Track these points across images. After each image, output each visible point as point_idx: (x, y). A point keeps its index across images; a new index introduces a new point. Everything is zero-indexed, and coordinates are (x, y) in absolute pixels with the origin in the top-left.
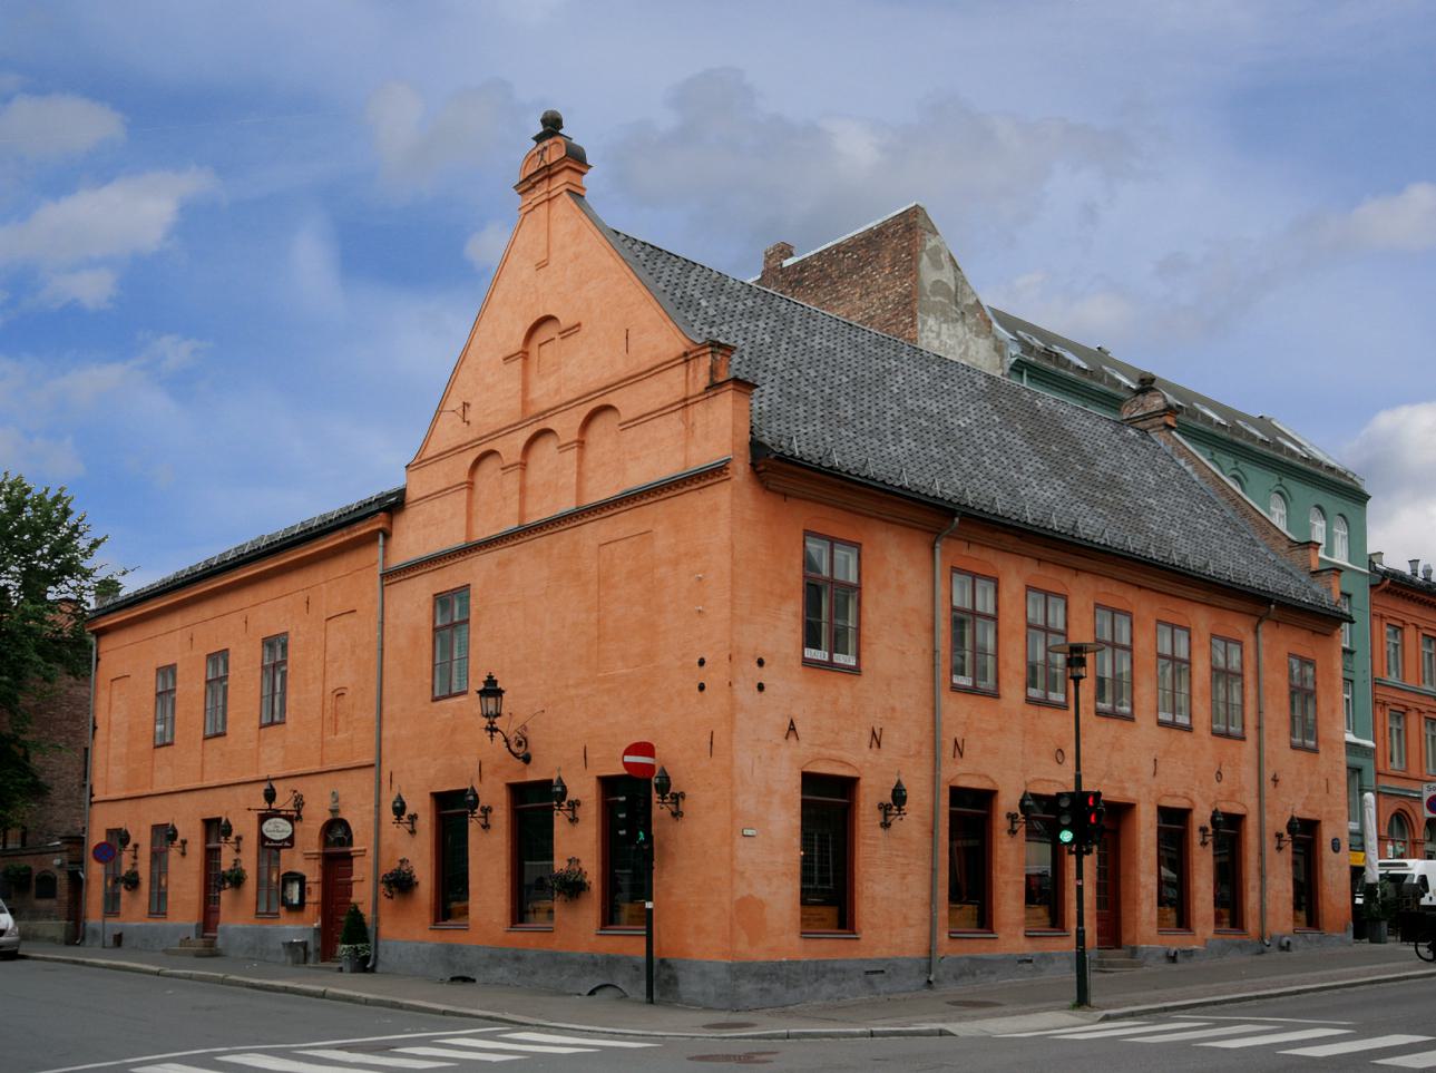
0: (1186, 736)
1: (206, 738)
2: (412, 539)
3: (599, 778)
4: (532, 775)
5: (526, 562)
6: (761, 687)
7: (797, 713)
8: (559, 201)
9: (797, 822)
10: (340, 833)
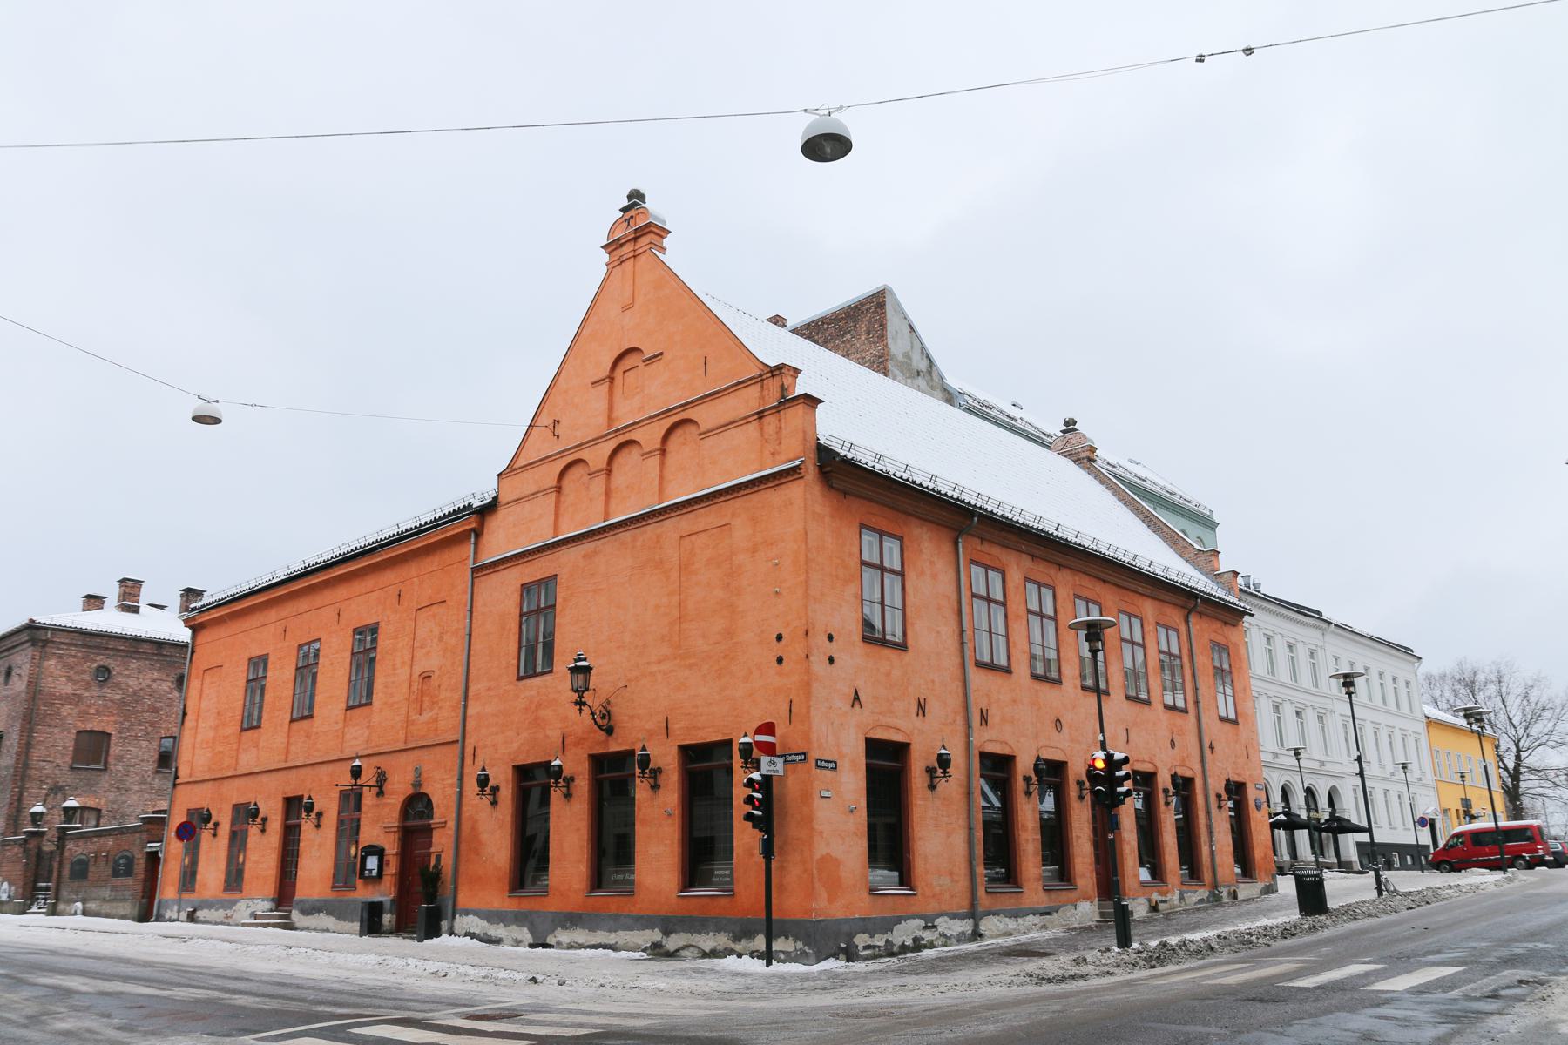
0: (1146, 708)
1: (292, 721)
2: (500, 540)
3: (680, 747)
4: (614, 747)
5: (613, 556)
6: (831, 660)
7: (860, 684)
8: (643, 257)
9: (863, 784)
10: (420, 807)
